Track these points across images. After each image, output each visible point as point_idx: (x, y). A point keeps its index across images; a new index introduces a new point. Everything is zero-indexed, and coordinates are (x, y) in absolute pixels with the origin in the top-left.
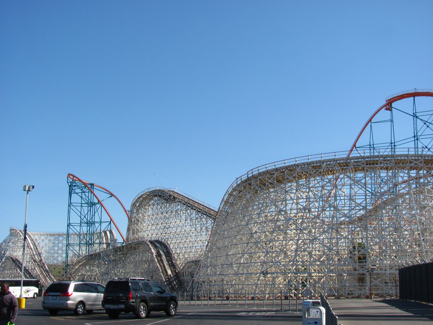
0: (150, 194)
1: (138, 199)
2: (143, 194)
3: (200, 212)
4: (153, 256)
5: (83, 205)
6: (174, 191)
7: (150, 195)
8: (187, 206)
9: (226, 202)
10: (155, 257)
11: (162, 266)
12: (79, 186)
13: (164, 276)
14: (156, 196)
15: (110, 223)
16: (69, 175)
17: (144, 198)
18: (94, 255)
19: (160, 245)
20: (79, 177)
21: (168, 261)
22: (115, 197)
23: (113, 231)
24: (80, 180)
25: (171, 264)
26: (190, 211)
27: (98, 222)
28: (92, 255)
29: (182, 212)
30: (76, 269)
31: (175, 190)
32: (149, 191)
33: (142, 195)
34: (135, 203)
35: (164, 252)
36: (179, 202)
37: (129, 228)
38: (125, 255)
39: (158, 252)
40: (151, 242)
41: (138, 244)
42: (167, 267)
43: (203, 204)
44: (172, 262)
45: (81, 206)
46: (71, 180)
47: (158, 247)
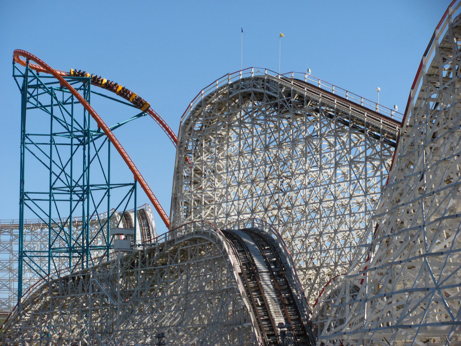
0: (230, 93)
1: (197, 109)
2: (212, 94)
3: (377, 138)
4: (233, 275)
5: (57, 139)
6: (303, 79)
7: (231, 96)
8: (339, 121)
9: (429, 75)
10: (237, 277)
11: (258, 306)
12: (47, 86)
13: (262, 335)
14: (246, 97)
15: (135, 187)
16: (18, 53)
17: (214, 104)
18: (73, 278)
19: (257, 244)
20: (42, 59)
21: (277, 291)
22: (154, 116)
23: (148, 213)
24: (48, 70)
25: (288, 298)
26: (349, 137)
27: (99, 187)
28: (66, 279)
29: (369, 166)
30: (29, 323)
31: (306, 76)
32: (227, 84)
33: (209, 97)
34: (187, 123)
35: (267, 264)
36: (317, 111)
37: (176, 199)
38: (159, 276)
39: (249, 263)
40: (229, 234)
41: (194, 241)
42: (273, 308)
43: (389, 116)
44: (290, 292)
45: (52, 142)
46: (23, 69)
47: (250, 248)
